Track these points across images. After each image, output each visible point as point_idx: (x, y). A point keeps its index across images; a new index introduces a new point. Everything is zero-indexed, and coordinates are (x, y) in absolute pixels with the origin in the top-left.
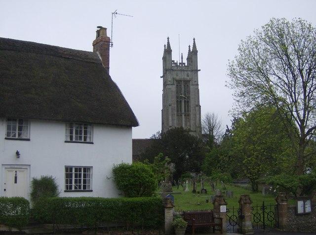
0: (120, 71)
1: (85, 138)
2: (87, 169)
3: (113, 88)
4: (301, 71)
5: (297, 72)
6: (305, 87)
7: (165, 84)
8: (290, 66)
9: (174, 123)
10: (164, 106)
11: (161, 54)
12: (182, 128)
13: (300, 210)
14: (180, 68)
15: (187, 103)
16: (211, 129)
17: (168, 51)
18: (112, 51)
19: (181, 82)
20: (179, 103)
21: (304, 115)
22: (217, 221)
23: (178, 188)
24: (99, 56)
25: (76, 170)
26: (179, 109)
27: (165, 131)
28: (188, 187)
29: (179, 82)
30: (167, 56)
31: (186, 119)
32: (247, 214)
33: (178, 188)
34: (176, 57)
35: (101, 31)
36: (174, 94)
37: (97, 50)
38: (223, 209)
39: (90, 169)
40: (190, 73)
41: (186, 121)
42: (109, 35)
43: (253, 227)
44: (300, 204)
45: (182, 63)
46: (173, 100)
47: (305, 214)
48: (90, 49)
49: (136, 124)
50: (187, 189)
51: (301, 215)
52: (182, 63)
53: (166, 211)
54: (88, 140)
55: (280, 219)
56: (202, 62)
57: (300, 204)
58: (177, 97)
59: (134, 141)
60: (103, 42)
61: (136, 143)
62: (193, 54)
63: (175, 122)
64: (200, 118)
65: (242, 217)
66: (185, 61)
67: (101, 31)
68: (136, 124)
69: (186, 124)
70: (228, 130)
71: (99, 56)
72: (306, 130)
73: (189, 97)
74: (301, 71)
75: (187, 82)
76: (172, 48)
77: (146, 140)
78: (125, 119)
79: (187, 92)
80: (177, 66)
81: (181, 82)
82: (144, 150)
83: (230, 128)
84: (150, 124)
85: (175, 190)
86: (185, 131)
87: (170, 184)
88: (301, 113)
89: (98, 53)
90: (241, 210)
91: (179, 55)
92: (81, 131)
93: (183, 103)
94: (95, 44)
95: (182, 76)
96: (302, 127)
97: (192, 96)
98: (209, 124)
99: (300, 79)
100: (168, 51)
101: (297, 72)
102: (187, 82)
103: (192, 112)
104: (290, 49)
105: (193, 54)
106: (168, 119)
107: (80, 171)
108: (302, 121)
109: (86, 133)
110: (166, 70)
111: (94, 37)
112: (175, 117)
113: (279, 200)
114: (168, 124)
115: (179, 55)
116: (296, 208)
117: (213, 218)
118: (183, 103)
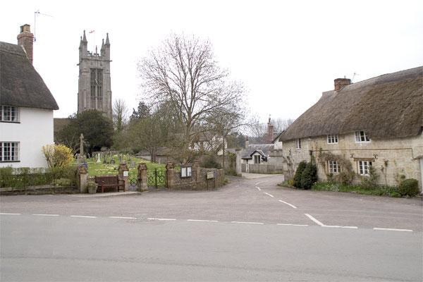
0: (40, 64)
1: (13, 119)
2: (17, 143)
3: (36, 77)
4: (190, 70)
5: (187, 70)
6: (192, 83)
7: (81, 72)
8: (182, 67)
9: (88, 106)
10: (80, 90)
11: (78, 44)
12: (95, 109)
13: (184, 175)
14: (94, 58)
15: (100, 88)
16: (120, 112)
17: (84, 43)
18: (35, 45)
19: (95, 72)
20: (93, 88)
21: (191, 104)
22: (121, 183)
23: (270, 119)
24: (24, 49)
25: (5, 144)
26: (93, 93)
27: (80, 112)
28: (99, 157)
29: (93, 70)
30: (83, 47)
31: (98, 102)
32: (144, 177)
33: (270, 119)
34: (91, 48)
35: (25, 28)
36: (89, 80)
37: (21, 44)
38: (126, 174)
39: (17, 144)
40: (103, 63)
41: (99, 104)
42: (32, 31)
43: (148, 186)
44: (184, 170)
45: (96, 54)
46: (88, 86)
47: (187, 177)
48: (15, 42)
49: (56, 107)
50: (99, 161)
51: (184, 178)
52: (96, 54)
53: (82, 175)
54: (15, 120)
55: (169, 181)
56: (113, 54)
57: (184, 170)
58: (92, 83)
59: (55, 119)
60: (26, 37)
61: (56, 121)
62: (106, 46)
63: (89, 104)
64: (111, 101)
65: (140, 180)
66: (99, 52)
67: (25, 28)
68: (56, 107)
69: (99, 107)
70: (134, 112)
71: (24, 49)
72: (192, 115)
73: (102, 84)
74: (190, 70)
75: (100, 71)
76: (88, 39)
77: (63, 119)
78: (52, 106)
79: (100, 78)
80: (92, 56)
81: (95, 72)
82: (65, 132)
83: (137, 110)
84: (68, 107)
85: (89, 162)
86: (99, 112)
87: (85, 156)
88: (189, 102)
89: (22, 46)
90: (140, 175)
91: (94, 47)
92: (9, 113)
93: (96, 88)
94: (19, 38)
95: (97, 65)
96: (190, 113)
97: (105, 83)
98: (119, 107)
99: (189, 76)
100: (84, 43)
101: (187, 70)
102: (100, 71)
103: (104, 96)
104: (183, 52)
105: (106, 46)
106: (83, 102)
107: (9, 144)
108: (190, 109)
109: (13, 114)
110: (82, 59)
111: (18, 32)
112: (90, 100)
113: (168, 167)
114: (83, 105)
115: (94, 47)
116: (180, 173)
117: (118, 181)
118: (96, 88)
